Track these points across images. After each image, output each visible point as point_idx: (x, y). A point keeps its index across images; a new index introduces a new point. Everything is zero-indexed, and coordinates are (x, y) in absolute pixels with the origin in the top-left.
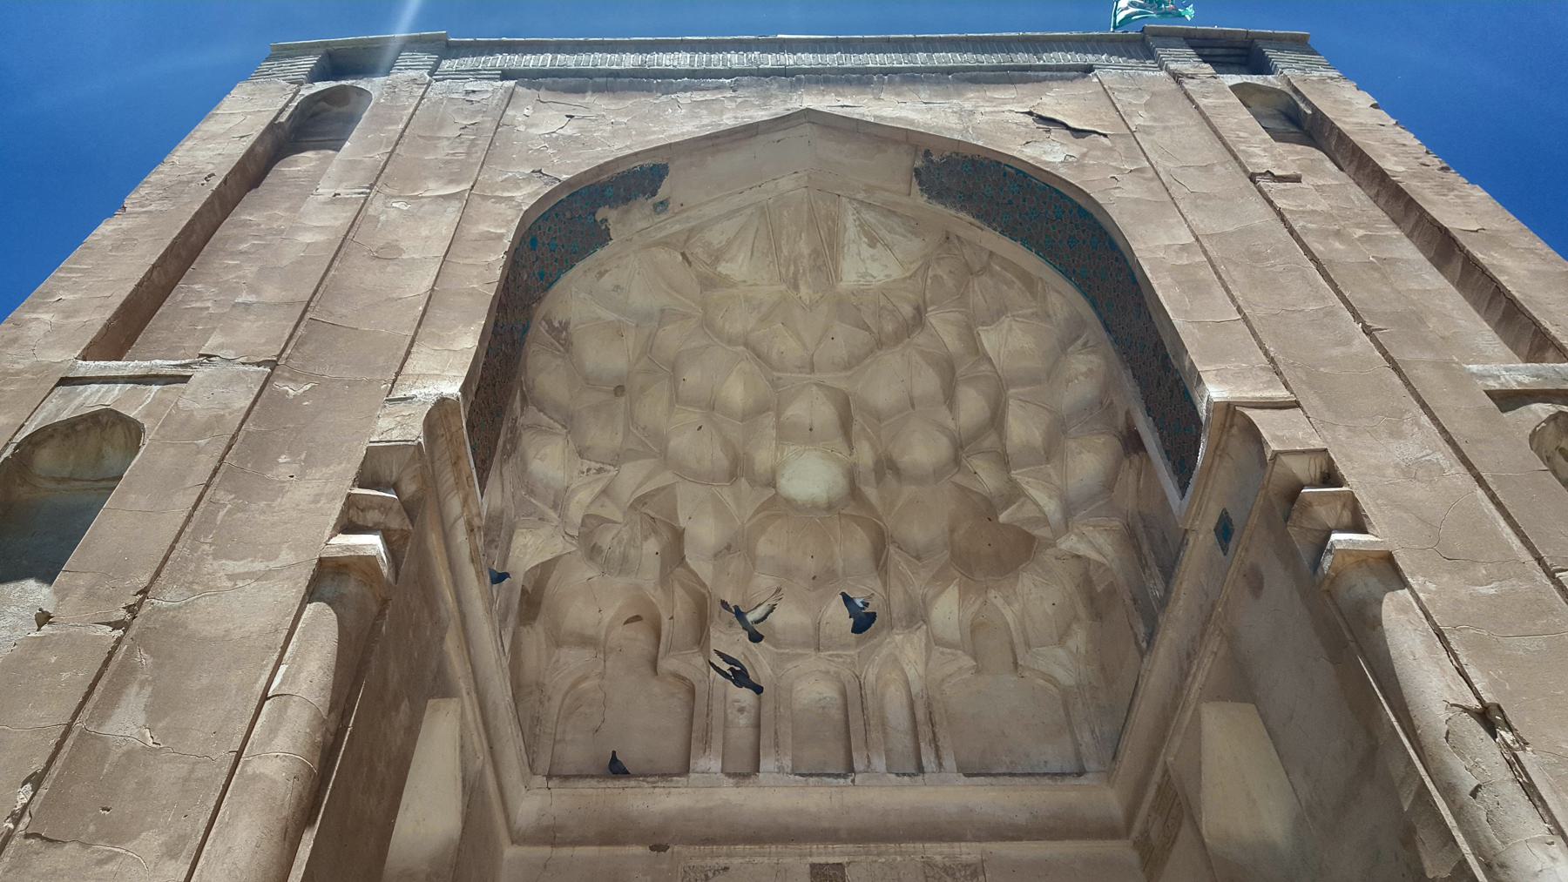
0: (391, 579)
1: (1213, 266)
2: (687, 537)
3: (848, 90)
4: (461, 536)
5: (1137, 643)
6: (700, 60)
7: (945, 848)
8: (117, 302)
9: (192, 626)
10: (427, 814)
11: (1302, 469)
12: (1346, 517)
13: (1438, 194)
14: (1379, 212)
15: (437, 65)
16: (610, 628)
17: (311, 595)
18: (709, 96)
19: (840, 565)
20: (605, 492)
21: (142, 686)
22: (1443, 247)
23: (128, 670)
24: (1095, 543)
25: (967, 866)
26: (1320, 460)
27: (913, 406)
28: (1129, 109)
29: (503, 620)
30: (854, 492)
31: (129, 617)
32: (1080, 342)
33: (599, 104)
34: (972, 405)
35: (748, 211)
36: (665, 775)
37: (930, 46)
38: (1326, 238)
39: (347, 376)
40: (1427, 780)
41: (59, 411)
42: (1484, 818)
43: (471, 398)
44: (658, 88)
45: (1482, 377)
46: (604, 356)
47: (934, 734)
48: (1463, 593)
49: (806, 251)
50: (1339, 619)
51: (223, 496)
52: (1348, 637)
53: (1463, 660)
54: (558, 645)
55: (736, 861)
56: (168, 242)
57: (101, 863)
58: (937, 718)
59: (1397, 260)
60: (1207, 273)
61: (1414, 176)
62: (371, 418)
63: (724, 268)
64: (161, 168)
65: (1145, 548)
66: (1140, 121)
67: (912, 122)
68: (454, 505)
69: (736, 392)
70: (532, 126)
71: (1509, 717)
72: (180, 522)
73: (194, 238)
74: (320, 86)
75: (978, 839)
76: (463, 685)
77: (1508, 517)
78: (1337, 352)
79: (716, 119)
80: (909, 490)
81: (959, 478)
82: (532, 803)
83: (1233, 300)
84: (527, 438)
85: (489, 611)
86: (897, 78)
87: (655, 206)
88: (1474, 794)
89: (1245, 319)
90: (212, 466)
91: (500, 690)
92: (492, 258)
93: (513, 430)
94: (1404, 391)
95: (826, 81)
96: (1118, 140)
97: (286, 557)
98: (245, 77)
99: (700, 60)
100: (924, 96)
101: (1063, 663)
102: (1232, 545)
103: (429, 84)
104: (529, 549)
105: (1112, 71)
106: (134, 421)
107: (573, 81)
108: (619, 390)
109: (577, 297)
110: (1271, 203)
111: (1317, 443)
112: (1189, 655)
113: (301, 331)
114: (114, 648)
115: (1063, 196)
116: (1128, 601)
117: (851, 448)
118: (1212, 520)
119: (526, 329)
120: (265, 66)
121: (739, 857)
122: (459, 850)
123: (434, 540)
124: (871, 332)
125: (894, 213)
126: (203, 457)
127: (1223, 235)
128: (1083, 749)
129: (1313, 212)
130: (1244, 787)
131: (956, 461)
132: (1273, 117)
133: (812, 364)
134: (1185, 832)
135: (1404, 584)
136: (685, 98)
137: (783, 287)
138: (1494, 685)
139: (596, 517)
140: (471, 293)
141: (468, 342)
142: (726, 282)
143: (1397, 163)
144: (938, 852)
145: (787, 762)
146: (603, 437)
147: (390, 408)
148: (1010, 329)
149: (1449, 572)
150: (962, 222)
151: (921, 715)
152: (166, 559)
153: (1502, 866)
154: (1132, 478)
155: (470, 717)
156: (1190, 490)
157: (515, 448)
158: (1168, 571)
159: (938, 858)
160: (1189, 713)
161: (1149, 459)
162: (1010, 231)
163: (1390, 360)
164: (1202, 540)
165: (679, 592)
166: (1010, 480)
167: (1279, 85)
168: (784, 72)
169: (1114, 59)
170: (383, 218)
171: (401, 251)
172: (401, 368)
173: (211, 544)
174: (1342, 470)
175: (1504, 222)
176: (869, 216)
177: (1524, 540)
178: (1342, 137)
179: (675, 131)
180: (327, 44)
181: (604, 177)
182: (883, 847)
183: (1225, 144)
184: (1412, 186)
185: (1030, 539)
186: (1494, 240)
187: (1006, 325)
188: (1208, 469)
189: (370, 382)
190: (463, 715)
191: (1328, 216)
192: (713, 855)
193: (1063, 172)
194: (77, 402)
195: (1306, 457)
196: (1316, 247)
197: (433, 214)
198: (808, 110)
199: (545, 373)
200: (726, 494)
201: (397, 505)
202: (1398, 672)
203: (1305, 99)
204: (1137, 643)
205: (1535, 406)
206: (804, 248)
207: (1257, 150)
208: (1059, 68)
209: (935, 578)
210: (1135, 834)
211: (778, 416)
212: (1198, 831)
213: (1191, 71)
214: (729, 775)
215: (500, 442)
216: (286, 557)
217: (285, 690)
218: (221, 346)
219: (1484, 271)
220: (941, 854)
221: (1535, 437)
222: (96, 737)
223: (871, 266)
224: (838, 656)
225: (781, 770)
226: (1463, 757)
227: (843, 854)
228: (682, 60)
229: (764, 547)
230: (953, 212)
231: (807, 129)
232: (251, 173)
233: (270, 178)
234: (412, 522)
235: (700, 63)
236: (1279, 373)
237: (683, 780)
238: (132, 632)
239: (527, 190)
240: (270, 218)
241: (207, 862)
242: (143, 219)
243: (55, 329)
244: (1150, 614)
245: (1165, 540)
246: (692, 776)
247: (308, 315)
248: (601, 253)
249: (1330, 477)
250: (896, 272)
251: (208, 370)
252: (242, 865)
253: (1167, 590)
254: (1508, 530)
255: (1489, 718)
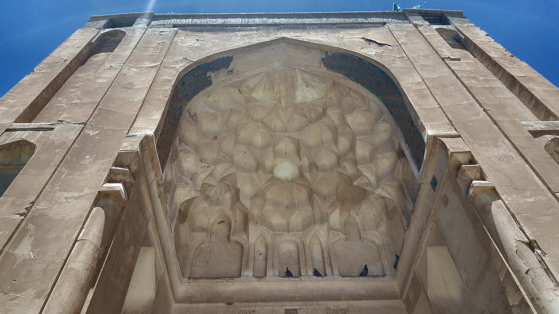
0: (126, 200)
1: (429, 89)
2: (241, 193)
3: (298, 31)
4: (155, 188)
5: (404, 227)
6: (245, 21)
7: (334, 303)
8: (29, 103)
9: (50, 216)
10: (141, 289)
11: (462, 158)
12: (478, 175)
13: (510, 64)
14: (489, 71)
15: (150, 23)
16: (213, 225)
17: (95, 204)
18: (248, 33)
19: (296, 202)
20: (210, 175)
21: (30, 236)
22: (512, 83)
23: (26, 231)
24: (388, 191)
25: (342, 309)
26: (468, 155)
27: (322, 144)
28: (399, 37)
29: (172, 220)
30: (301, 175)
31: (26, 212)
32: (382, 119)
33: (208, 36)
34: (344, 143)
35: (263, 74)
36: (232, 278)
37: (328, 16)
38: (470, 79)
39: (112, 128)
40: (509, 269)
41: (5, 140)
42: (531, 282)
43: (158, 137)
44: (230, 30)
45: (527, 126)
46: (210, 126)
47: (330, 262)
48: (521, 201)
49: (284, 89)
50: (476, 211)
51: (63, 169)
52: (479, 218)
53: (522, 225)
54: (194, 231)
55: (258, 308)
56: (49, 83)
57: (11, 300)
58: (332, 256)
59: (496, 88)
60: (427, 92)
61: (501, 58)
62: (120, 142)
63: (254, 95)
64: (48, 58)
65: (406, 192)
66: (402, 41)
67: (321, 41)
68: (152, 176)
69: (259, 140)
70: (184, 43)
71: (539, 245)
72: (48, 179)
73: (59, 82)
74: (107, 30)
75: (346, 300)
76: (156, 242)
77: (537, 174)
78: (474, 118)
79: (250, 40)
80: (321, 174)
81: (339, 170)
82: (183, 288)
83: (436, 100)
84: (181, 155)
85: (166, 216)
86: (316, 27)
87: (228, 72)
88: (527, 273)
89: (441, 107)
90: (60, 159)
91: (170, 246)
92: (167, 88)
93: (176, 151)
94: (498, 131)
95: (290, 28)
96: (395, 47)
97: (87, 191)
98: (80, 27)
99: (245, 21)
100: (325, 33)
101: (377, 236)
102: (437, 188)
103: (147, 29)
104: (182, 195)
105: (392, 24)
106: (33, 144)
107: (198, 28)
108: (215, 138)
109: (199, 104)
110: (450, 68)
111: (467, 149)
112: (422, 230)
113: (96, 112)
114: (20, 223)
115: (375, 66)
116: (400, 212)
117: (300, 159)
118: (429, 179)
119: (180, 115)
120: (88, 24)
121: (258, 307)
122: (154, 303)
123: (144, 188)
124: (307, 118)
125: (315, 75)
126: (57, 156)
127: (433, 79)
128: (385, 267)
129: (465, 70)
130: (443, 278)
131: (338, 163)
132: (451, 40)
133: (286, 129)
134: (422, 295)
135: (499, 198)
136: (239, 34)
137: (275, 102)
138: (533, 233)
139: (207, 184)
140: (159, 100)
141: (157, 116)
142: (255, 100)
143: (495, 54)
144: (332, 304)
145: (277, 272)
146: (210, 155)
147: (127, 139)
148: (357, 115)
149: (516, 194)
150: (340, 77)
151: (326, 255)
152: (42, 191)
153: (537, 299)
154: (401, 167)
155: (158, 254)
156: (421, 169)
157: (176, 158)
158: (414, 200)
159: (332, 307)
160: (423, 252)
161: (407, 160)
162: (357, 80)
163: (493, 120)
164: (426, 188)
165: (238, 212)
166: (358, 170)
167: (453, 29)
168: (275, 25)
169: (393, 20)
170: (128, 74)
171: (134, 85)
172: (132, 125)
173: (59, 187)
174: (476, 159)
175: (534, 74)
176: (306, 76)
177: (544, 182)
178: (475, 46)
179: (235, 45)
180: (111, 16)
181: (210, 61)
182: (311, 303)
183: (433, 48)
184: (501, 62)
185: (365, 191)
186: (530, 79)
187: (355, 114)
188: (428, 160)
189: (120, 130)
190: (156, 253)
191: (471, 72)
192: (249, 306)
193: (375, 58)
194: (12, 137)
195: (463, 154)
196: (466, 82)
197: (146, 73)
198: (283, 37)
199: (188, 131)
200: (255, 176)
201: (129, 173)
202: (499, 232)
203: (462, 33)
204: (404, 227)
205: (546, 136)
206: (283, 88)
207: (444, 50)
208: (374, 23)
209: (331, 206)
210: (404, 297)
211: (274, 148)
212: (426, 294)
213: (421, 24)
214: (255, 277)
215: (170, 154)
216: (87, 191)
217: (84, 238)
218: (66, 118)
219: (527, 90)
220: (333, 305)
221: (547, 147)
222: (12, 254)
223: (307, 94)
224: (296, 234)
225: (274, 275)
226: (522, 259)
227: (297, 305)
228: (238, 21)
229: (269, 195)
230: (336, 74)
231: (283, 44)
232: (82, 59)
233: (88, 62)
234: (135, 180)
235: (245, 22)
236: (453, 126)
237: (238, 279)
238: (28, 217)
239: (181, 65)
240: (88, 75)
241: (52, 299)
242: (41, 75)
243: (6, 112)
244: (408, 216)
245: (413, 189)
246: (242, 278)
247: (99, 107)
248: (209, 88)
249: (472, 161)
250: (316, 96)
251: (61, 126)
252: (65, 301)
253: (414, 206)
254: (537, 179)
255: (532, 245)
